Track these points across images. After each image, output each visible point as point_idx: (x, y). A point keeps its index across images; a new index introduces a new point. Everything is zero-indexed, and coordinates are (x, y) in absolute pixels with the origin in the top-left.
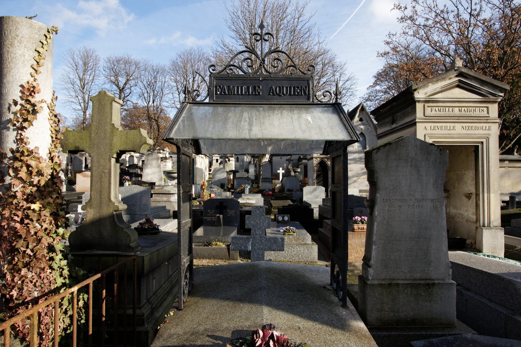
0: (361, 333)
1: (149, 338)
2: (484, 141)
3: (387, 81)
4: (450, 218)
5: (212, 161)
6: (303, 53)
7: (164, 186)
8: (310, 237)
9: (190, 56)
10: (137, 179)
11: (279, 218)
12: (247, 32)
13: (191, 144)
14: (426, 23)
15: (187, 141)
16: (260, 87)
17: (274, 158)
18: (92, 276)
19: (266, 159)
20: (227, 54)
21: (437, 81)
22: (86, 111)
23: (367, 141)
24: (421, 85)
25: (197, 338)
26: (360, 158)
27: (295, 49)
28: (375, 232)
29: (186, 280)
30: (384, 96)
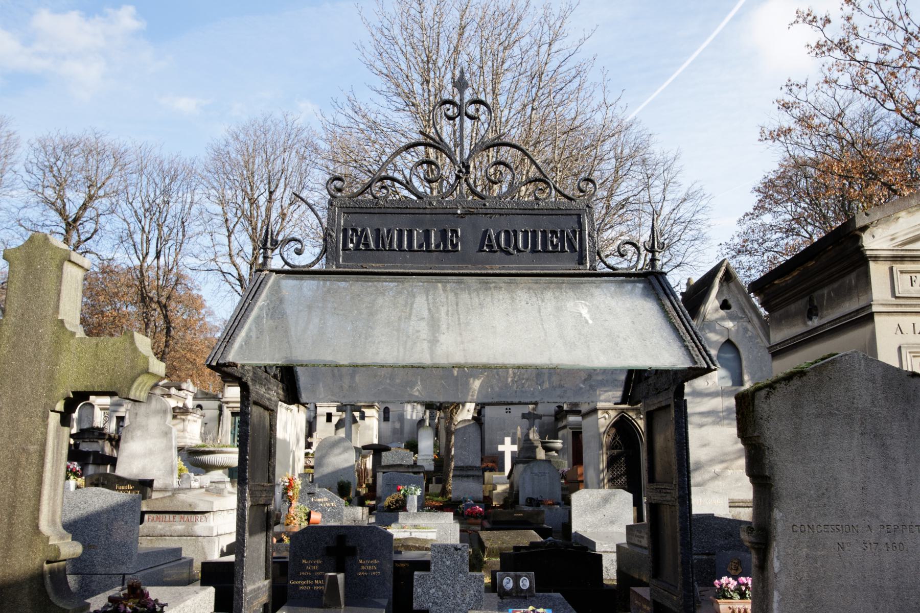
3: (792, 201)
5: (315, 418)
6: (565, 129)
7: (179, 489)
10: (101, 469)
11: (505, 581)
12: (416, 76)
13: (275, 376)
14: (881, 56)
15: (266, 369)
16: (456, 232)
20: (362, 131)
23: (744, 363)
24: (877, 215)
26: (728, 410)
27: (543, 121)
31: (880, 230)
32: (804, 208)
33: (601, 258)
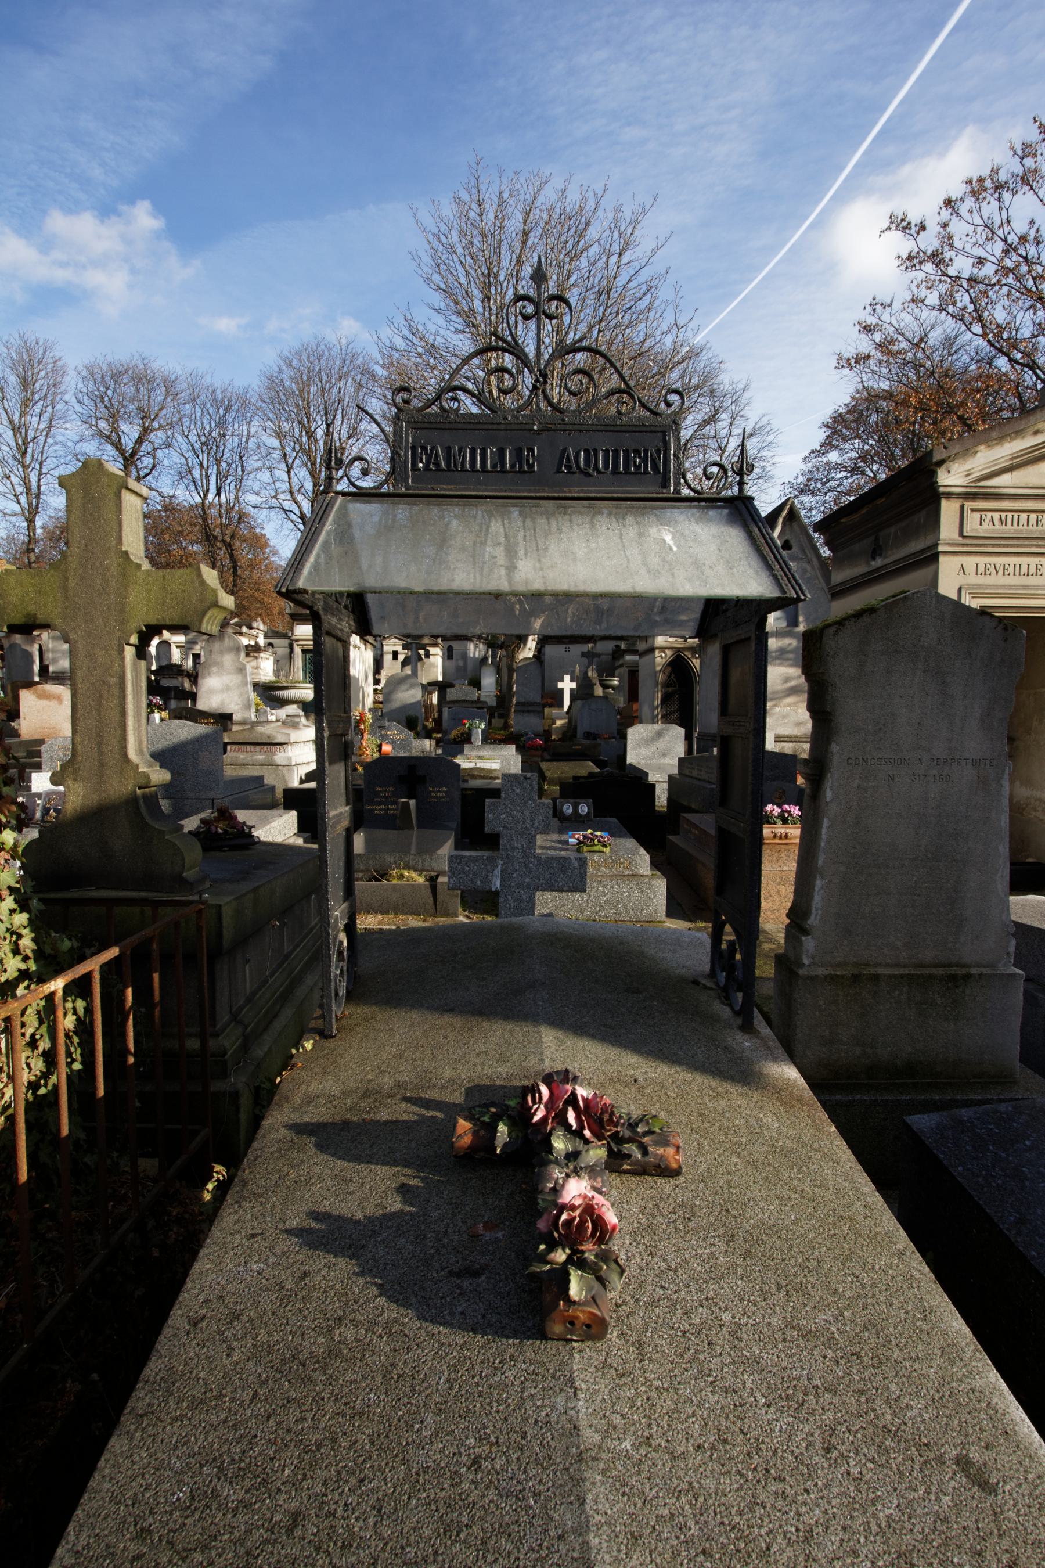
0: (791, 1092)
1: (242, 1110)
4: (1017, 809)
5: (382, 656)
6: (633, 354)
7: (257, 722)
8: (647, 857)
9: (317, 362)
10: (183, 704)
11: (565, 807)
12: (476, 292)
13: (346, 607)
15: (337, 596)
17: (549, 650)
18: (93, 954)
19: (528, 650)
20: (420, 355)
21: (1001, 439)
22: (34, 516)
24: (957, 448)
25: (377, 1104)
28: (823, 844)
29: (341, 964)
30: (850, 480)
31: (956, 465)
32: (871, 446)
33: (686, 481)
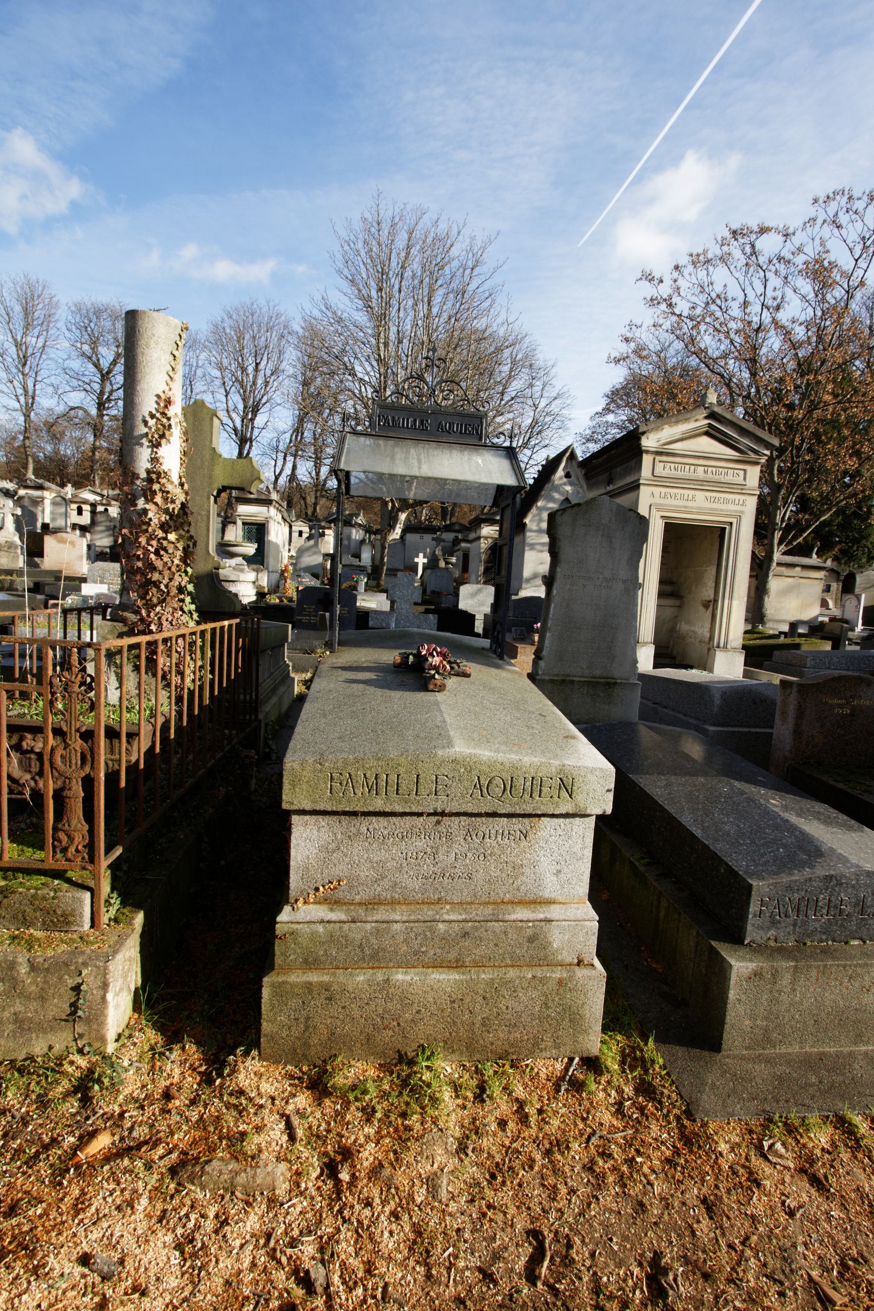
2: (734, 521)
12: (373, 284)
19: (396, 534)
21: (677, 422)
24: (653, 426)
